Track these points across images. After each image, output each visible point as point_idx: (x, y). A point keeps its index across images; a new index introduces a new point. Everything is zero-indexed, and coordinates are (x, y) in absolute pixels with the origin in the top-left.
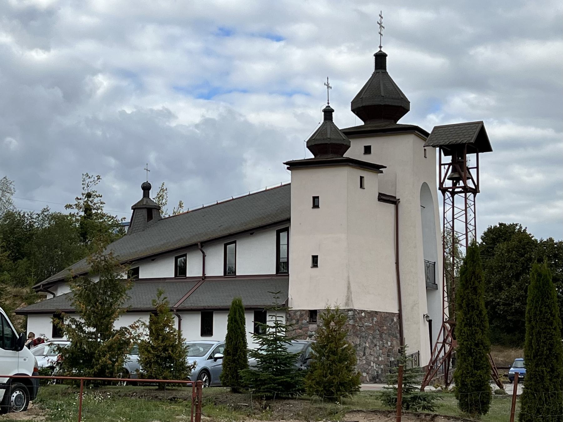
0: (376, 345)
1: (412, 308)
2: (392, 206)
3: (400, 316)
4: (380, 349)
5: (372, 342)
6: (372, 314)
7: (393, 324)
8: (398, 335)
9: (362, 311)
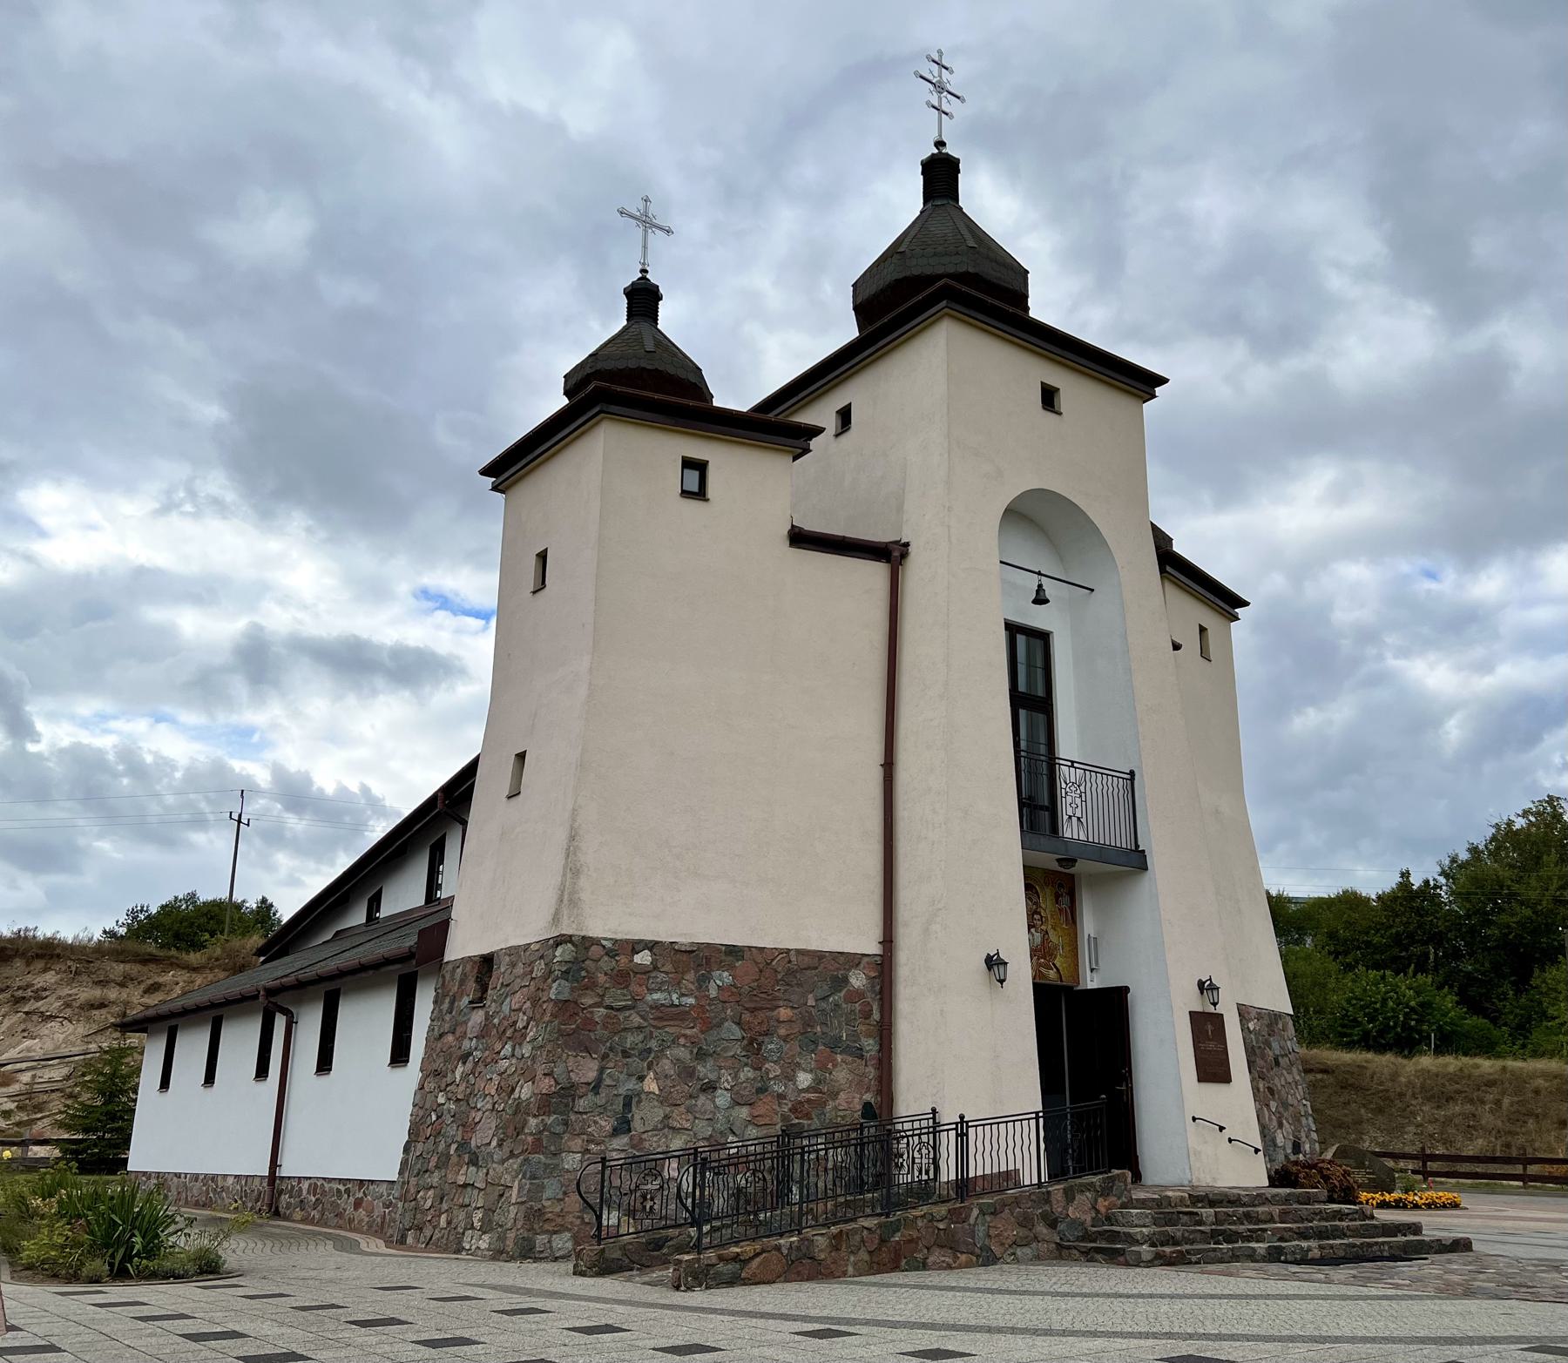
0: (710, 1088)
1: (926, 931)
2: (876, 572)
3: (884, 967)
4: (736, 1103)
5: (688, 1073)
6: (699, 959)
7: (838, 997)
8: (870, 1045)
9: (635, 946)
